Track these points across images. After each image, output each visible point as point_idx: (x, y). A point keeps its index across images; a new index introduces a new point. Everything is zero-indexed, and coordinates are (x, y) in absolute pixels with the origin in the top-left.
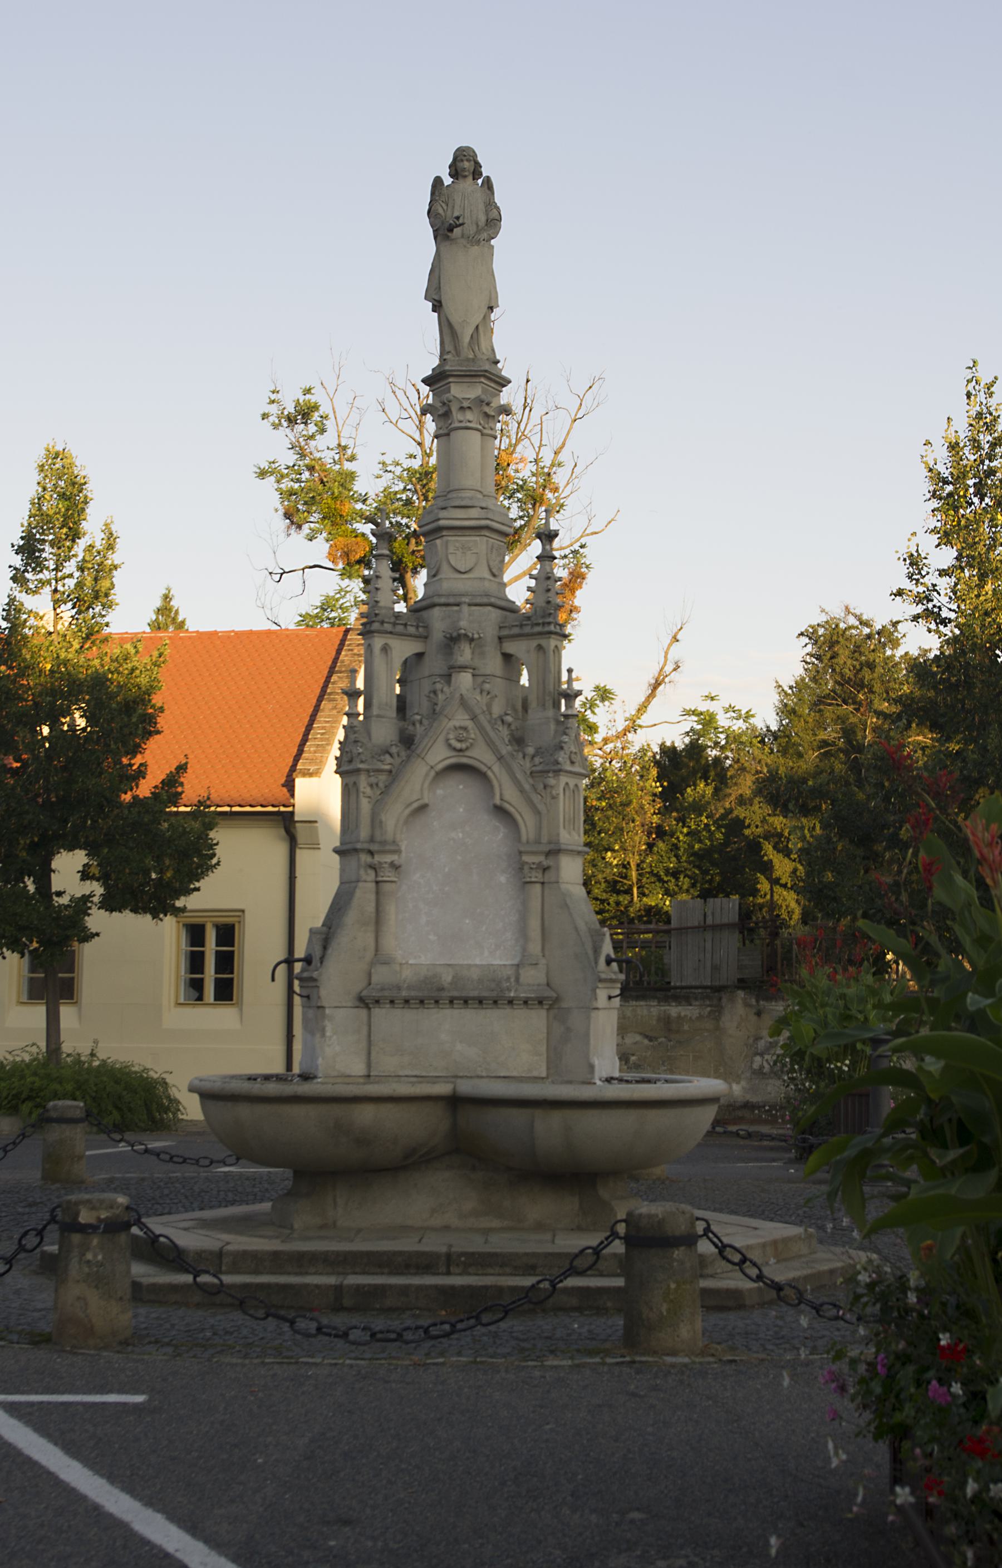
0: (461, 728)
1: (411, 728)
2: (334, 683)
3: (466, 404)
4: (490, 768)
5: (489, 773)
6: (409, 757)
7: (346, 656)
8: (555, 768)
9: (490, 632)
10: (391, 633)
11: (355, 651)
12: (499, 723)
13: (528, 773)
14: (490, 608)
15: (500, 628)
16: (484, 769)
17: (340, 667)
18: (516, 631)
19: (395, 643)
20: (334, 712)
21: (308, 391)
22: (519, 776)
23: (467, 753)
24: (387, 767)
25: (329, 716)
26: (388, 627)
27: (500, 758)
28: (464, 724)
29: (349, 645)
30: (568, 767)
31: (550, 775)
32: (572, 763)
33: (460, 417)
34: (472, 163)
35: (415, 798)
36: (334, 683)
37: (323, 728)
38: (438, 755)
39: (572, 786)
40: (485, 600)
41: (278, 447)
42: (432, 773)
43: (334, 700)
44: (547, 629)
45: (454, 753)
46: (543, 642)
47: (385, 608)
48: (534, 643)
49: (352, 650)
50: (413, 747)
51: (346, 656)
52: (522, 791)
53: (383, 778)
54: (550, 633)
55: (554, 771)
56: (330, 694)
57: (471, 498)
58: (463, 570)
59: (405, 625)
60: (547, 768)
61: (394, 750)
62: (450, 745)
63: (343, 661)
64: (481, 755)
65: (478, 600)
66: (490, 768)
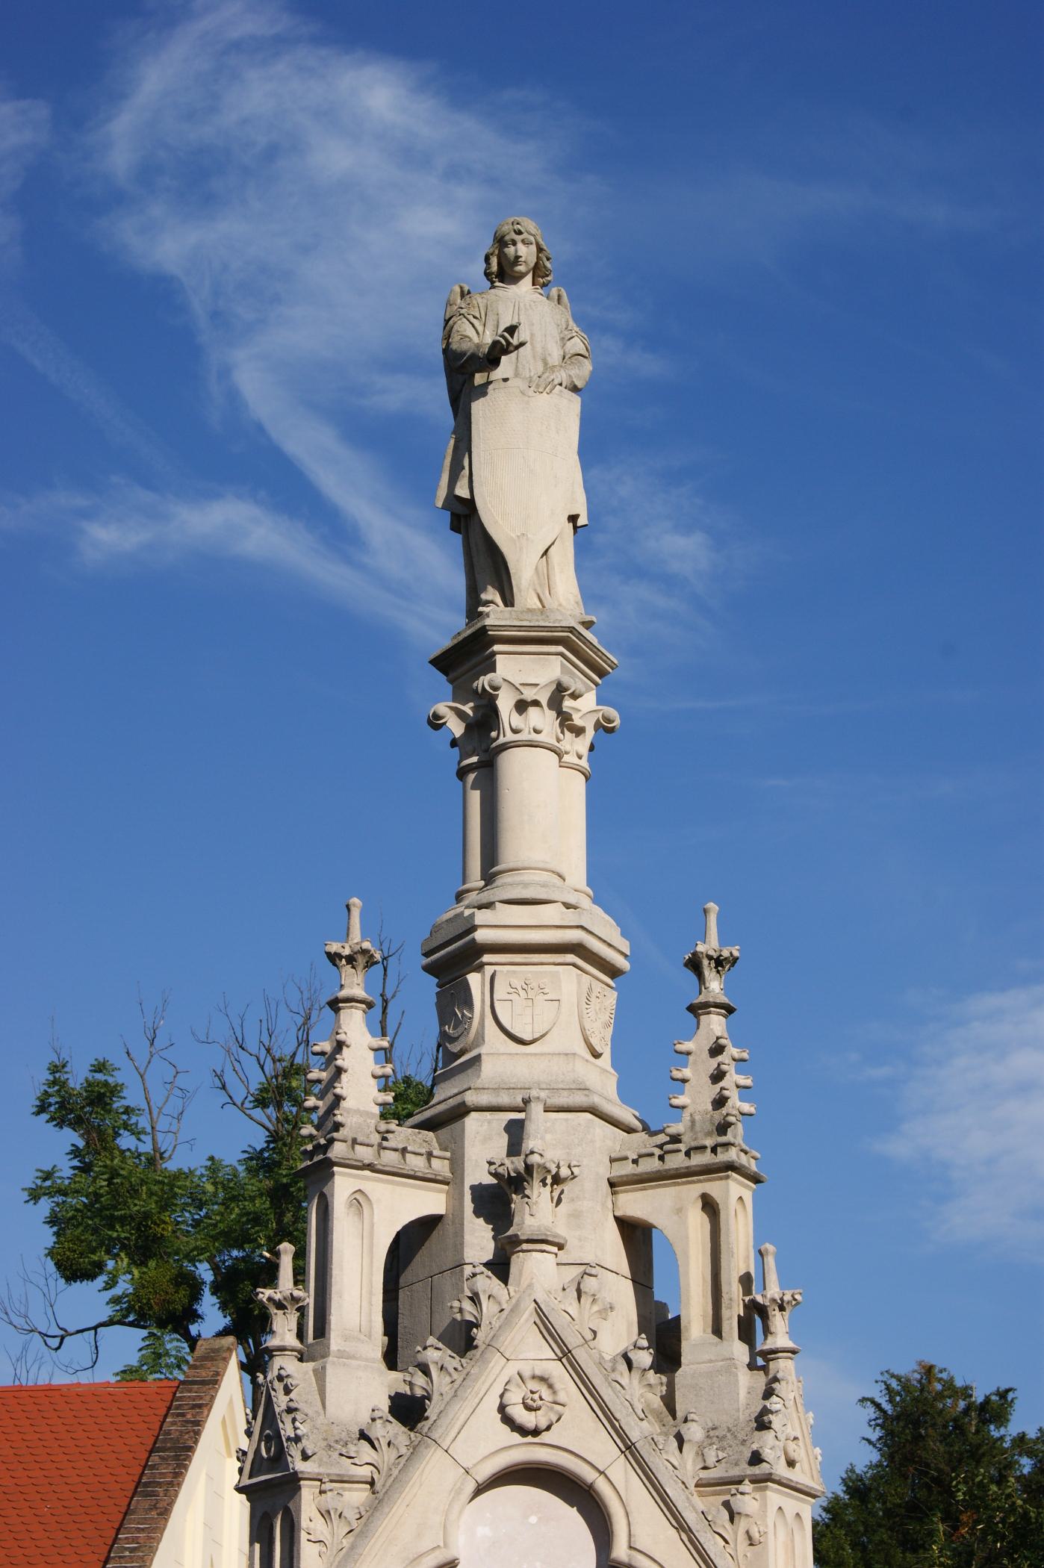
0: (543, 1379)
1: (420, 1380)
2: (153, 1467)
3: (529, 694)
4: (602, 1473)
5: (602, 1486)
6: (415, 1448)
7: (173, 1423)
8: (757, 1470)
9: (594, 1171)
10: (370, 1167)
11: (189, 1416)
12: (623, 1366)
13: (691, 1484)
14: (588, 1115)
15: (612, 1160)
16: (588, 1475)
17: (165, 1441)
18: (651, 1165)
19: (376, 1187)
20: (154, 1513)
21: (100, 1067)
22: (673, 1491)
23: (545, 1437)
24: (366, 1472)
25: (144, 1521)
26: (365, 1154)
27: (629, 1448)
28: (540, 1369)
29: (178, 1407)
30: (781, 1470)
31: (747, 1487)
32: (791, 1463)
33: (517, 720)
34: (533, 248)
35: (427, 1544)
36: (153, 1467)
37: (134, 1540)
38: (487, 1444)
39: (790, 1514)
40: (579, 1099)
41: (57, 1147)
42: (471, 1487)
43: (154, 1494)
44: (723, 1157)
45: (516, 1438)
46: (713, 1187)
47: (358, 1111)
48: (693, 1190)
49: (183, 1415)
50: (423, 1426)
51: (173, 1423)
52: (681, 1526)
53: (357, 1497)
54: (731, 1167)
55: (755, 1480)
56: (146, 1485)
57: (544, 885)
58: (527, 1037)
59: (404, 1151)
60: (735, 1472)
61: (378, 1431)
62: (508, 1420)
63: (168, 1433)
64: (580, 1441)
65: (564, 1100)
66: (602, 1473)
